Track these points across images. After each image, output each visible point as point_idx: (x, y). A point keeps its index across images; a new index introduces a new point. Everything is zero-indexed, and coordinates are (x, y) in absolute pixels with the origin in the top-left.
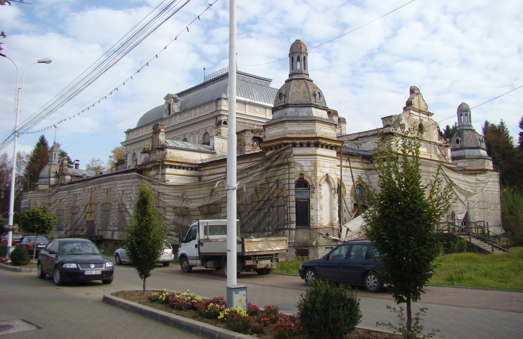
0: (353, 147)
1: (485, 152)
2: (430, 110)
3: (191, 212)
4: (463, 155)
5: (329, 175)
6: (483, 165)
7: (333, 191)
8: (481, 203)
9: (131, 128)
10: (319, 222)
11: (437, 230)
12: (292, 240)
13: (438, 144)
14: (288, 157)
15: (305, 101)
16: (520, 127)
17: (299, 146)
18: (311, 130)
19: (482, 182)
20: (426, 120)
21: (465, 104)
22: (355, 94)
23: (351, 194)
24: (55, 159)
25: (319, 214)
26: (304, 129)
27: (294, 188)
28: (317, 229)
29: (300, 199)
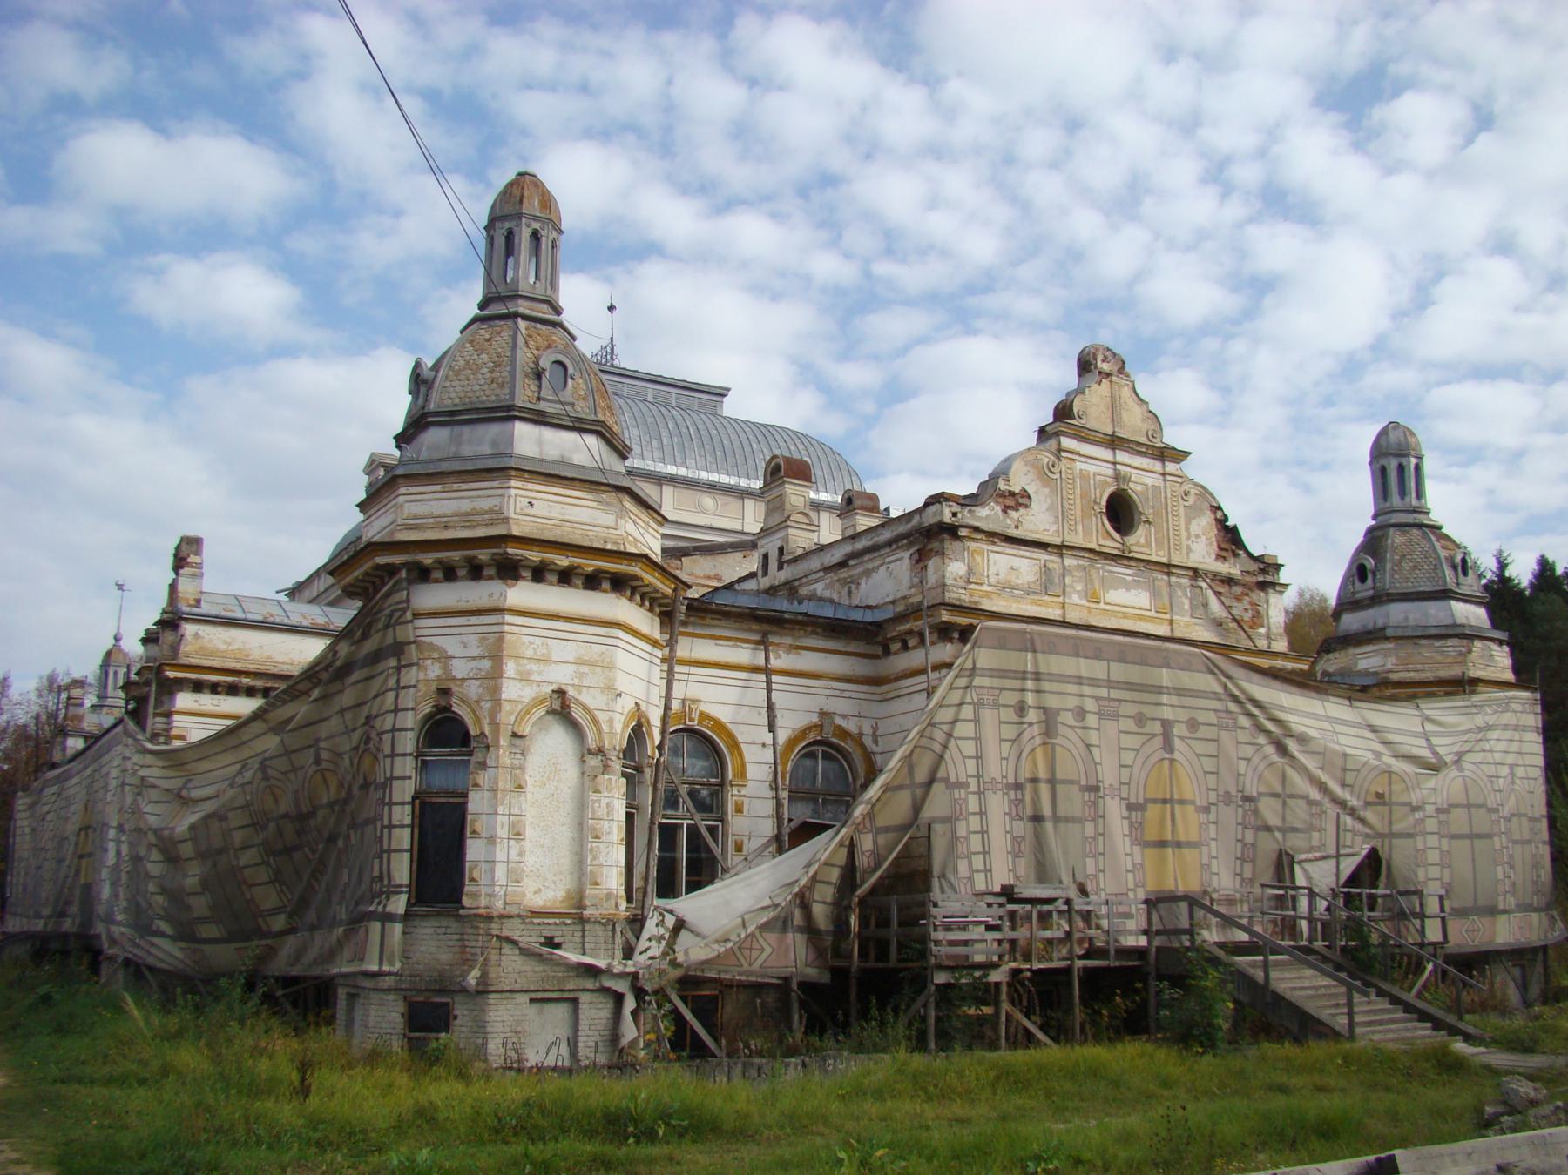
0: (835, 597)
1: (1481, 612)
4: (1380, 623)
5: (571, 692)
6: (1464, 663)
7: (594, 762)
8: (1456, 813)
9: (302, 579)
12: (392, 964)
15: (489, 396)
17: (438, 574)
18: (490, 512)
22: (1308, 489)
25: (500, 855)
26: (465, 506)
28: (489, 918)
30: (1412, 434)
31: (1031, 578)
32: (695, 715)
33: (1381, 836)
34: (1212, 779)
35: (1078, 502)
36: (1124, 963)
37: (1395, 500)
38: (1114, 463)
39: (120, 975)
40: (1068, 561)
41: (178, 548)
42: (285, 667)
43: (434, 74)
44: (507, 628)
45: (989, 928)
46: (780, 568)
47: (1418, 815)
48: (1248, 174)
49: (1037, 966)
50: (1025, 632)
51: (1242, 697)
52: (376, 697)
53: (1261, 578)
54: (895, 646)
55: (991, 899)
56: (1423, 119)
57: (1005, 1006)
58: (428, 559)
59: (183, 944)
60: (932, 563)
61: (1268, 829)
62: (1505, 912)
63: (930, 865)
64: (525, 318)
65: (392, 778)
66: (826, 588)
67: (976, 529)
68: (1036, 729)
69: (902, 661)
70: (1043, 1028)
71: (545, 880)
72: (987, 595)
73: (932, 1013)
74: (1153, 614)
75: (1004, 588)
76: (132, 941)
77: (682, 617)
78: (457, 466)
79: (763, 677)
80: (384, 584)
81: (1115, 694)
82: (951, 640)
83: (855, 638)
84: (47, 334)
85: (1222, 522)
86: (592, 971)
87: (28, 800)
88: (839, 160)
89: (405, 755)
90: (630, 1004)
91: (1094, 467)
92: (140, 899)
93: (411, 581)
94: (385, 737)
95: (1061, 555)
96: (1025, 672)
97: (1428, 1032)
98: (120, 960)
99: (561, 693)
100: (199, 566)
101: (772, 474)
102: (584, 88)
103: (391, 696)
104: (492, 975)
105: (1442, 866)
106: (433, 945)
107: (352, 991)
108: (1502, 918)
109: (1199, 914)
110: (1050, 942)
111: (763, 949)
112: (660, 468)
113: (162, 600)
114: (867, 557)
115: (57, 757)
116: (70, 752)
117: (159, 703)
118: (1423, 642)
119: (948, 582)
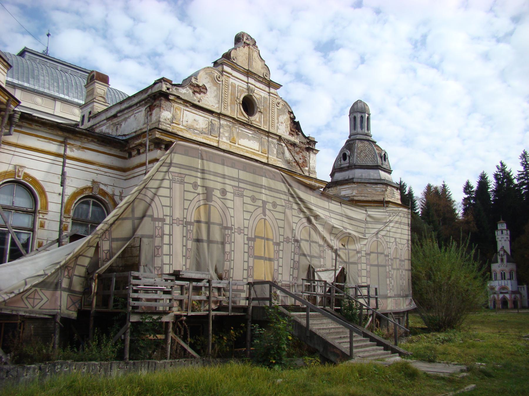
2: (274, 77)
4: (351, 177)
6: (384, 195)
8: (373, 255)
11: (247, 299)
13: (288, 141)
16: (465, 192)
19: (377, 221)
20: (264, 94)
21: (361, 101)
30: (367, 105)
31: (204, 126)
32: (21, 174)
33: (345, 262)
34: (281, 230)
35: (229, 96)
36: (236, 314)
37: (359, 130)
38: (248, 83)
40: (222, 122)
45: (166, 292)
46: (89, 121)
47: (359, 255)
48: (291, 68)
49: (190, 313)
50: (198, 149)
51: (295, 196)
53: (307, 146)
54: (134, 153)
55: (167, 277)
56: (344, 57)
57: (171, 334)
60: (154, 112)
61: (304, 255)
62: (390, 297)
63: (139, 260)
66: (107, 128)
67: (178, 97)
68: (201, 197)
69: (137, 160)
70: (192, 346)
72: (181, 130)
73: (128, 338)
74: (260, 153)
75: (189, 128)
77: (17, 120)
79: (62, 160)
81: (241, 185)
82: (160, 149)
85: (293, 119)
88: (161, 49)
91: (238, 83)
95: (219, 118)
96: (197, 168)
97: (382, 352)
101: (91, 79)
102: (77, 13)
105: (367, 277)
108: (389, 300)
109: (274, 289)
110: (200, 302)
111: (42, 299)
112: (56, 94)
118: (368, 185)
119: (162, 120)
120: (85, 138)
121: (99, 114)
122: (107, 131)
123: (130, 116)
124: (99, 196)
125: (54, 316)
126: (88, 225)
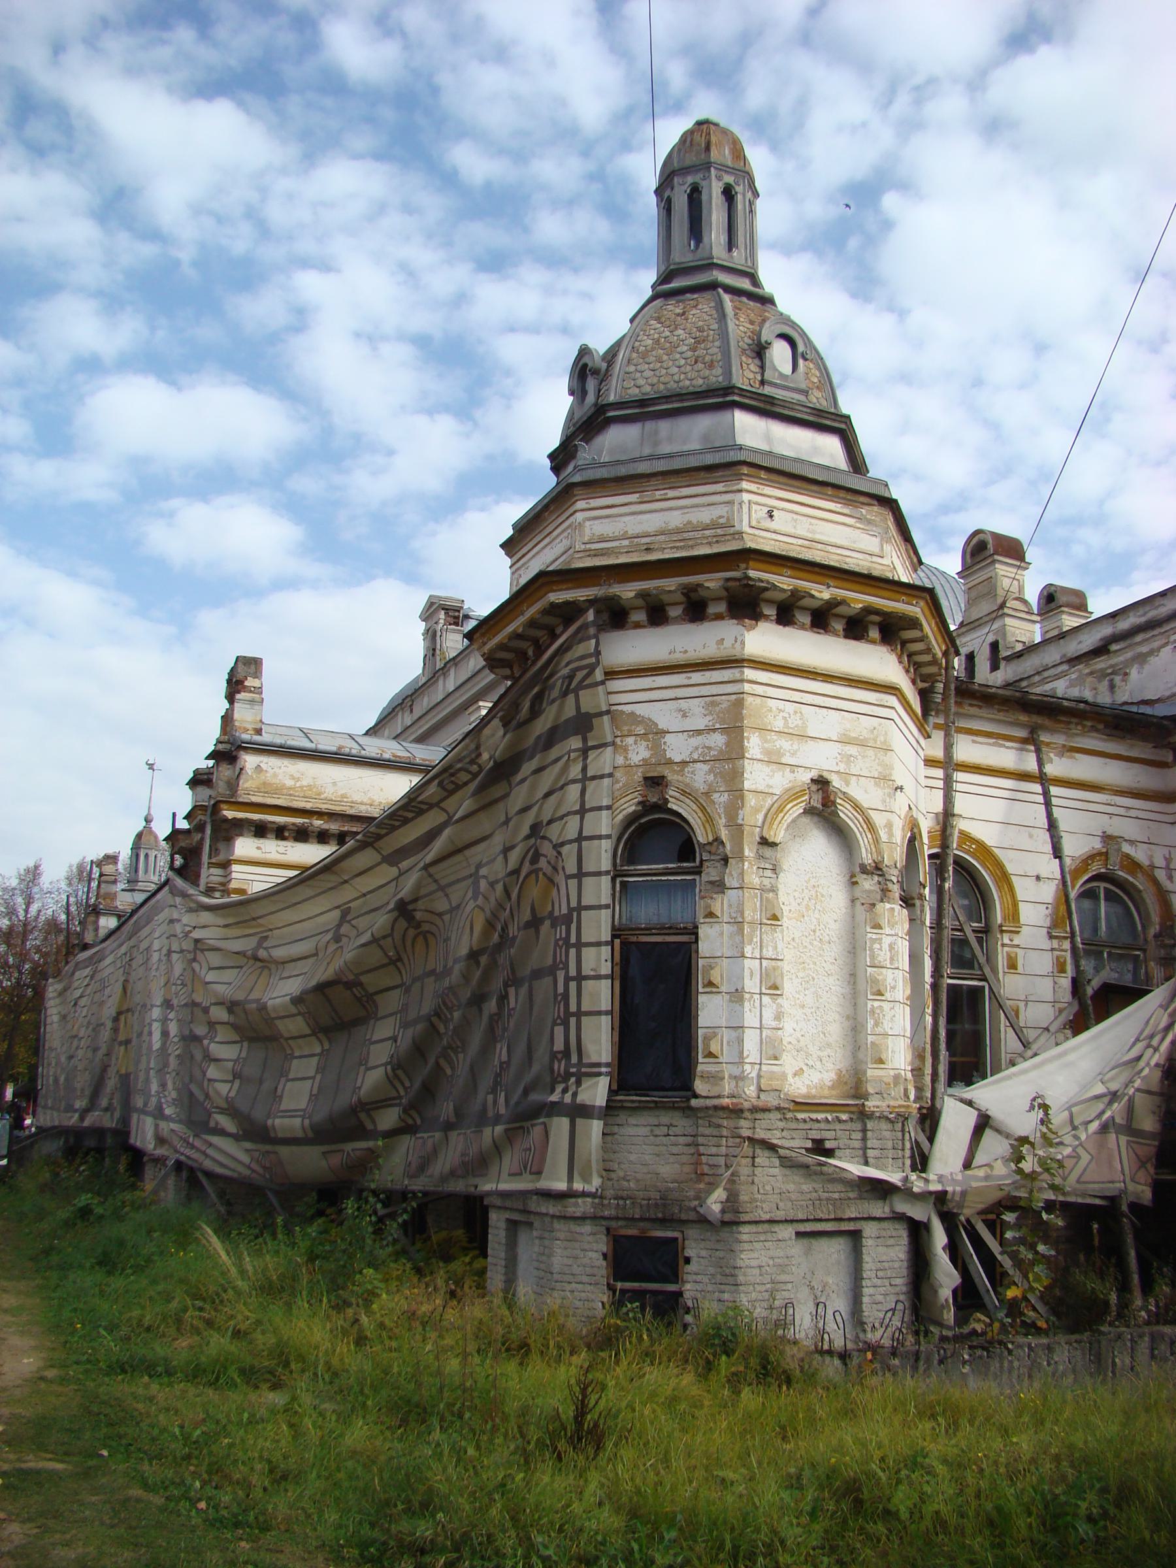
3: (280, 1024)
5: (836, 782)
7: (868, 884)
10: (750, 1071)
12: (586, 1179)
14: (581, 686)
15: (695, 379)
17: (640, 616)
18: (713, 525)
23: (1055, 924)
24: (146, 871)
25: (750, 1018)
27: (606, 864)
28: (736, 1112)
29: (648, 930)
39: (171, 1182)
41: (232, 672)
42: (363, 808)
43: (423, 321)
44: (747, 687)
46: (995, 667)
52: (548, 795)
58: (627, 591)
59: (248, 1145)
64: (729, 290)
65: (580, 908)
66: (1072, 685)
71: (808, 1055)
76: (186, 1141)
78: (661, 466)
80: (554, 637)
83: (1144, 739)
84: (72, 574)
86: (880, 1189)
87: (59, 987)
89: (599, 874)
90: (939, 1237)
92: (194, 1088)
93: (602, 628)
94: (565, 850)
98: (170, 1163)
99: (821, 783)
100: (259, 690)
103: (574, 791)
104: (743, 1197)
106: (649, 1152)
107: (516, 1216)
113: (215, 731)
114: (1139, 638)
115: (89, 938)
116: (102, 933)
117: (214, 851)
120: (1077, 724)
121: (1031, 649)
122: (1075, 693)
123: (1159, 649)
124: (1121, 873)
125: (1113, 1200)
126: (1101, 953)
